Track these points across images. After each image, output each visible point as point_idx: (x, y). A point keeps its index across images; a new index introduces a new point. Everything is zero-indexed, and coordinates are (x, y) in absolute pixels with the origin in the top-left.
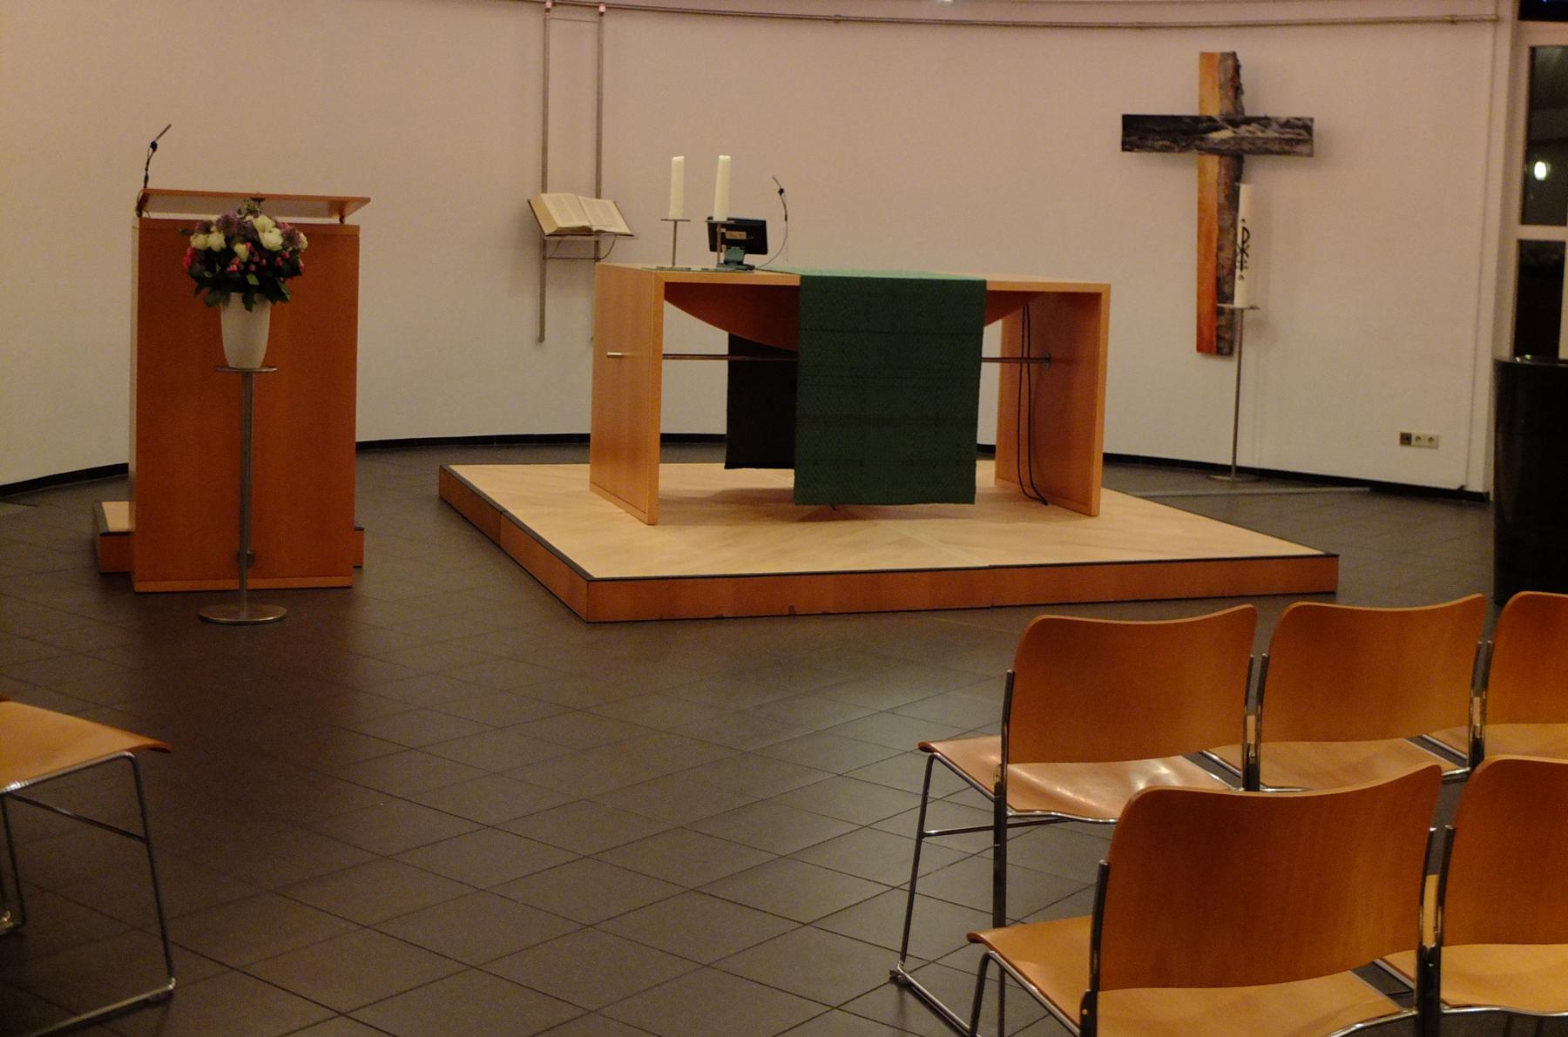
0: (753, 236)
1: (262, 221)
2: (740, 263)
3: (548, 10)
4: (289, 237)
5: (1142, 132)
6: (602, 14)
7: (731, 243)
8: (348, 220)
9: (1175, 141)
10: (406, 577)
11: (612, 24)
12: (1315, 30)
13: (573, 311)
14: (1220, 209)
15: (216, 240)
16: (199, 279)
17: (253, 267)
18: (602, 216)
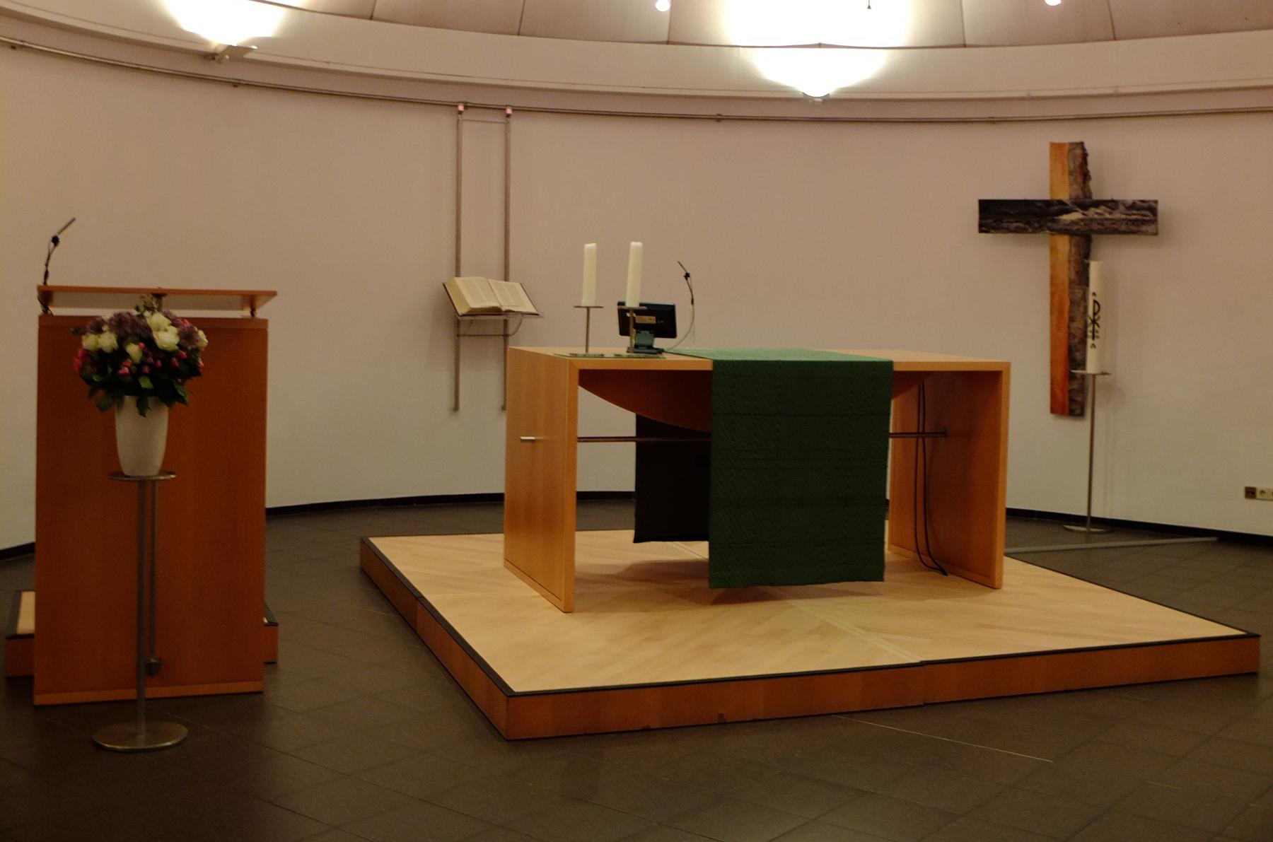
0: (661, 320)
1: (156, 320)
2: (650, 347)
3: (460, 113)
4: (187, 337)
5: (997, 216)
6: (508, 116)
7: (640, 328)
8: (260, 314)
9: (1028, 223)
10: (322, 672)
11: (517, 124)
12: (1153, 121)
13: (484, 382)
14: (1071, 283)
15: (107, 341)
16: (89, 381)
17: (146, 369)
18: (510, 297)
